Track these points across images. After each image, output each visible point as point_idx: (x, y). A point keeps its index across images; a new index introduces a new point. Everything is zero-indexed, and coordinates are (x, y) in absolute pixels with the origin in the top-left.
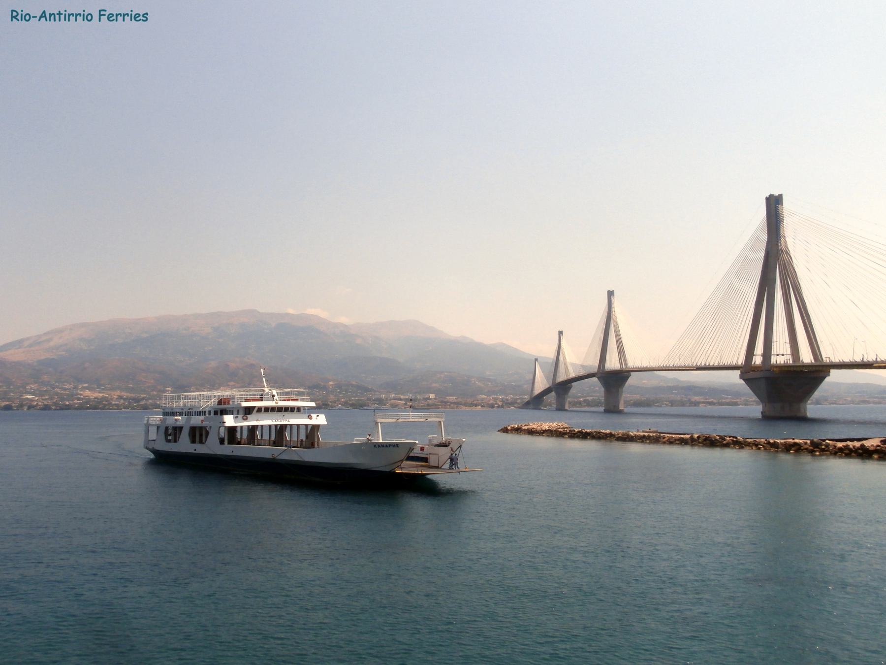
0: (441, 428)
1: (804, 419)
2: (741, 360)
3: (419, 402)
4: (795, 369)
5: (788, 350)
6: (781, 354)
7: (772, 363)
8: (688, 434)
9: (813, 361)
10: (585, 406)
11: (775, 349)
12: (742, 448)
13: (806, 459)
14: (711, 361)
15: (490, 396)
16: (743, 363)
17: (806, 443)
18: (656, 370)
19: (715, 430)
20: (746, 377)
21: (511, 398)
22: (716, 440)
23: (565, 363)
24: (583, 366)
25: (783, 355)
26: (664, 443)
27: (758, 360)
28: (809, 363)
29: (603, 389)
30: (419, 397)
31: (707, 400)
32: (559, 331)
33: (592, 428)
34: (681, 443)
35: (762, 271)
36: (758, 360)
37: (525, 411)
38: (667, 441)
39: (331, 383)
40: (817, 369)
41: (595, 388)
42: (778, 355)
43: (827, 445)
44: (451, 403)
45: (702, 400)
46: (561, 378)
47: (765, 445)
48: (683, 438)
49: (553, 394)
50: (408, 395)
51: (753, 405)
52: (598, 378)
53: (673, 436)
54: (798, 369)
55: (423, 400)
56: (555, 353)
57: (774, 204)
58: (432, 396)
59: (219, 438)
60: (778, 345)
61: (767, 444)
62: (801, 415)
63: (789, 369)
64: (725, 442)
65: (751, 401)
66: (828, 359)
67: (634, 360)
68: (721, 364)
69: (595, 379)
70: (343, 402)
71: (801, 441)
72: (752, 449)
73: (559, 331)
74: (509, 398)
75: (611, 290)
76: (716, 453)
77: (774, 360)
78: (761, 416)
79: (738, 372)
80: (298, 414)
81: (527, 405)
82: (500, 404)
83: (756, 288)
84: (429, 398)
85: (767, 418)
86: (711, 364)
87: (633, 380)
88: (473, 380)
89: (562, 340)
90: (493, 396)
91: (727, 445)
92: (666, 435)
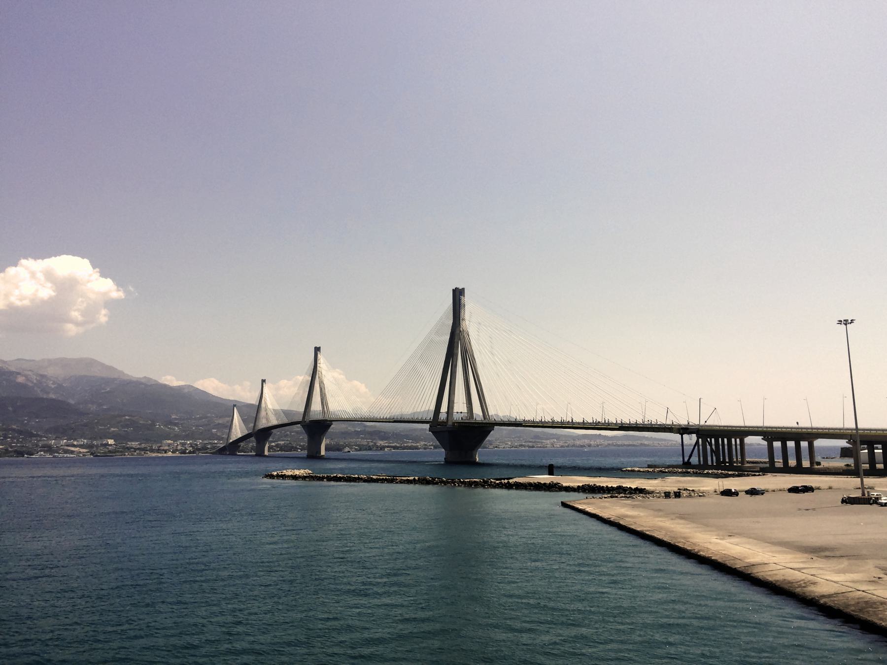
0: (339, 485)
2: (431, 416)
3: (97, 449)
10: (278, 451)
13: (480, 490)
15: (176, 441)
16: (432, 419)
17: (480, 481)
25: (461, 413)
26: (397, 483)
30: (95, 443)
31: (391, 445)
32: (262, 380)
34: (408, 483)
37: (220, 458)
38: (399, 481)
41: (286, 432)
43: (491, 482)
45: (387, 445)
46: (263, 424)
49: (253, 439)
50: (82, 441)
53: (403, 478)
55: (100, 447)
56: (258, 397)
57: (458, 294)
58: (111, 442)
65: (430, 446)
71: (478, 480)
74: (198, 443)
75: (318, 347)
79: (427, 426)
81: (222, 451)
84: (107, 444)
85: (448, 462)
87: (495, 434)
88: (158, 424)
89: (264, 388)
90: (180, 441)
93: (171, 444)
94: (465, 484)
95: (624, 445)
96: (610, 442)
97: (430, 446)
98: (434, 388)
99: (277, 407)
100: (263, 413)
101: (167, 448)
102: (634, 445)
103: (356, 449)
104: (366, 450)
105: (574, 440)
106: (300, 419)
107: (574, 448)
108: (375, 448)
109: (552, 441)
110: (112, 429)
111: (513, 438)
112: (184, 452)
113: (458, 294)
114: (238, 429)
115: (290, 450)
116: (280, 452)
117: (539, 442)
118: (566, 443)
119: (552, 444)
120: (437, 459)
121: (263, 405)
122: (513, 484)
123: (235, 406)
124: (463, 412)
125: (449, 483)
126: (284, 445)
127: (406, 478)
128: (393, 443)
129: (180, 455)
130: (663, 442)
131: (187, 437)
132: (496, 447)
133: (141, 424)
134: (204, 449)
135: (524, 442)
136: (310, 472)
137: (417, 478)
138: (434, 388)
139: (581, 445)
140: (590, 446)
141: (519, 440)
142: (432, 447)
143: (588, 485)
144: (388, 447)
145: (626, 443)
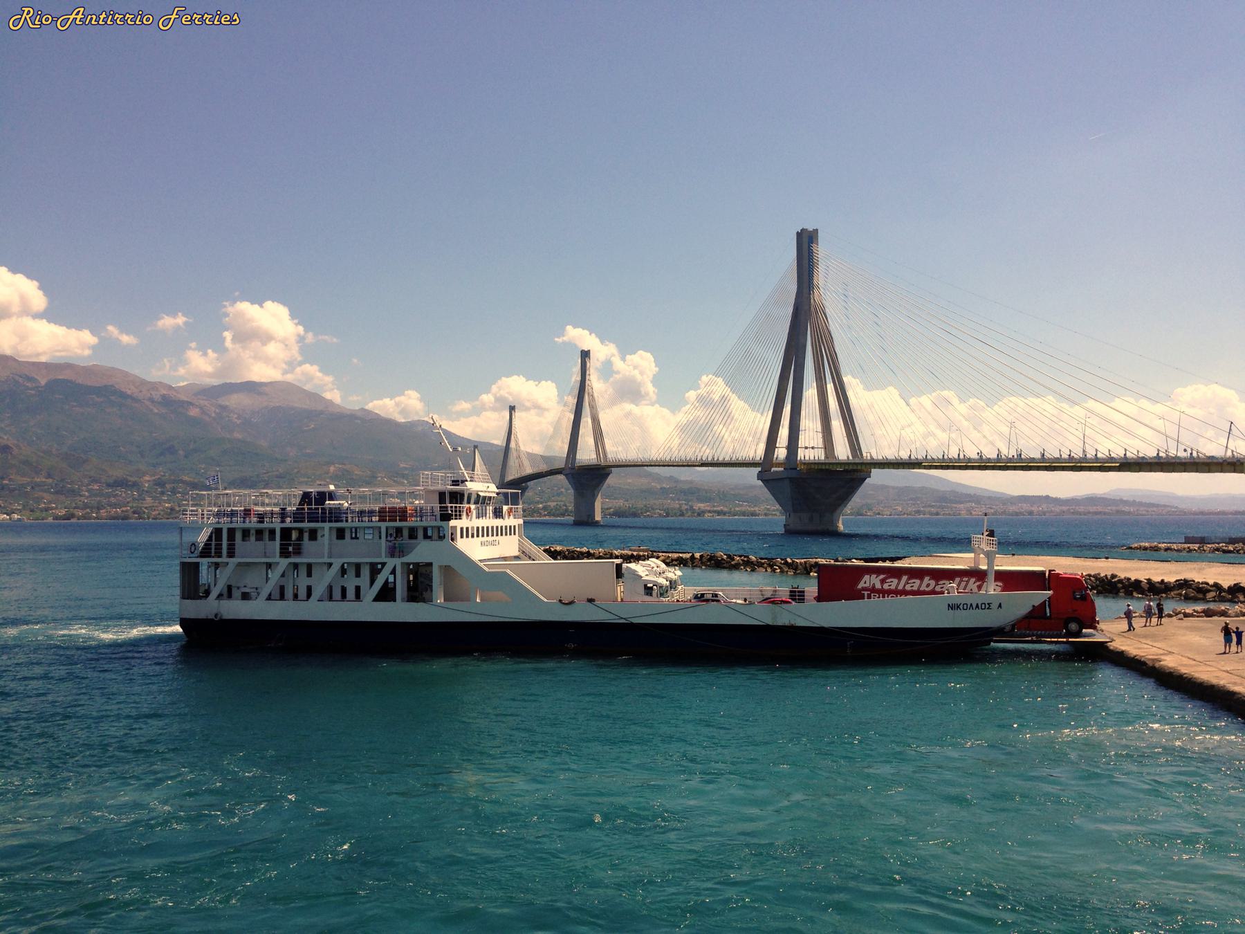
1: (836, 534)
2: (758, 451)
5: (818, 440)
6: (811, 448)
7: (799, 458)
9: (851, 458)
10: (545, 515)
11: (803, 440)
12: (753, 570)
14: (721, 453)
18: (647, 466)
22: (723, 559)
23: (518, 450)
24: (544, 458)
25: (813, 448)
28: (893, 460)
29: (571, 491)
32: (510, 406)
35: (789, 333)
36: (781, 453)
39: (147, 478)
40: (855, 467)
42: (806, 448)
45: (708, 509)
47: (782, 566)
51: (775, 515)
52: (566, 475)
57: (806, 242)
60: (807, 435)
61: (784, 564)
62: (831, 529)
63: (820, 467)
66: (868, 455)
67: (616, 450)
68: (733, 459)
69: (561, 477)
70: (167, 508)
72: (766, 571)
73: (510, 406)
75: (586, 350)
77: (802, 454)
78: (784, 530)
80: (454, 534)
83: (780, 357)
85: (790, 532)
86: (721, 459)
87: (877, 477)
91: (736, 567)
94: (796, 569)
95: (1089, 513)
96: (1065, 508)
100: (512, 461)
102: (1105, 513)
103: (660, 514)
105: (1004, 504)
106: (560, 464)
107: (1004, 517)
108: (690, 513)
109: (968, 505)
111: (905, 501)
113: (806, 242)
115: (562, 515)
116: (547, 518)
117: (947, 507)
118: (991, 508)
119: (968, 511)
121: (513, 445)
122: (128, 395)
123: (476, 447)
125: (761, 565)
127: (676, 556)
128: (718, 506)
130: (1155, 509)
132: (879, 514)
133: (356, 474)
135: (923, 507)
137: (697, 555)
139: (1016, 512)
140: (1031, 513)
141: (914, 504)
142: (778, 514)
143: (1095, 576)
144: (709, 512)
145: (1092, 509)
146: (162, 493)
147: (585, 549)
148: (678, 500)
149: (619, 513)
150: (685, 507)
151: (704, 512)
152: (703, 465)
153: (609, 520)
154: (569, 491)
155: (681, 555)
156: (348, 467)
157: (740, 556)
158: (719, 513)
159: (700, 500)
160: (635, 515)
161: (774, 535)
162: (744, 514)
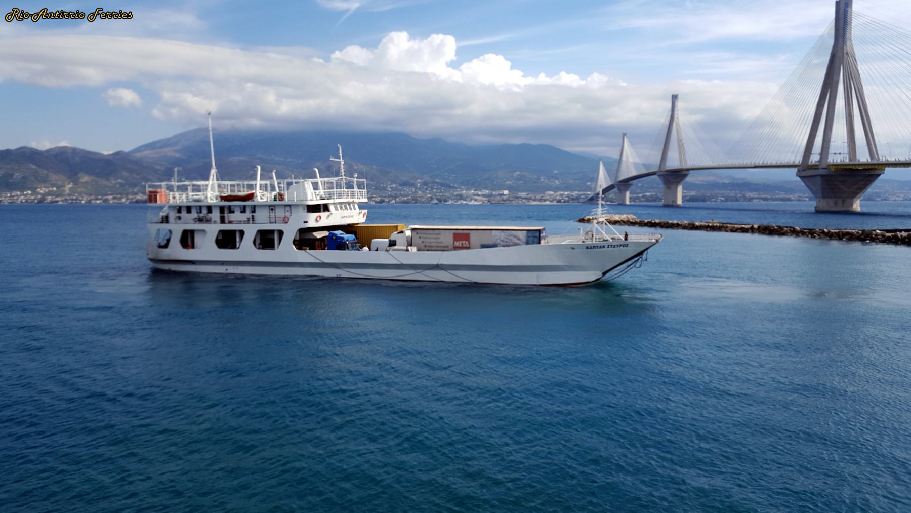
2: (798, 159)
4: (851, 167)
6: (839, 154)
8: (748, 224)
10: (643, 201)
13: (857, 245)
15: (557, 192)
19: (774, 223)
20: (804, 174)
21: (576, 194)
24: (645, 165)
27: (815, 158)
30: (494, 193)
33: (660, 219)
39: (419, 181)
44: (523, 198)
45: (756, 196)
48: (744, 228)
49: (616, 190)
52: (659, 176)
54: (854, 167)
59: (527, 243)
64: (783, 232)
76: (776, 239)
79: (795, 170)
82: (567, 199)
84: (503, 194)
91: (784, 234)
92: (729, 225)
93: (552, 195)
97: (805, 197)
98: (803, 133)
99: (638, 160)
101: (548, 197)
103: (722, 201)
104: (732, 201)
108: (742, 200)
110: (507, 182)
112: (559, 201)
114: (603, 180)
120: (810, 209)
121: (624, 158)
124: (842, 152)
126: (651, 196)
127: (740, 226)
129: (556, 204)
131: (566, 189)
134: (577, 199)
136: (635, 217)
138: (803, 133)
142: (807, 199)
146: (427, 189)
147: (675, 222)
148: (735, 191)
149: (692, 199)
150: (739, 195)
151: (753, 198)
152: (756, 167)
153: (688, 204)
154: (660, 186)
155: (744, 226)
156: (524, 173)
157: (787, 227)
158: (764, 199)
159: (751, 191)
160: (704, 200)
161: (812, 213)
162: (782, 199)
